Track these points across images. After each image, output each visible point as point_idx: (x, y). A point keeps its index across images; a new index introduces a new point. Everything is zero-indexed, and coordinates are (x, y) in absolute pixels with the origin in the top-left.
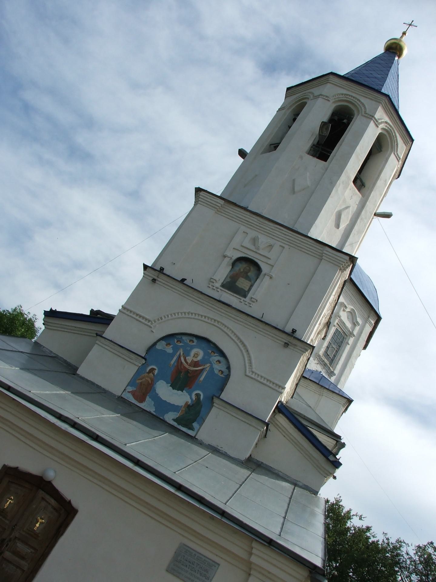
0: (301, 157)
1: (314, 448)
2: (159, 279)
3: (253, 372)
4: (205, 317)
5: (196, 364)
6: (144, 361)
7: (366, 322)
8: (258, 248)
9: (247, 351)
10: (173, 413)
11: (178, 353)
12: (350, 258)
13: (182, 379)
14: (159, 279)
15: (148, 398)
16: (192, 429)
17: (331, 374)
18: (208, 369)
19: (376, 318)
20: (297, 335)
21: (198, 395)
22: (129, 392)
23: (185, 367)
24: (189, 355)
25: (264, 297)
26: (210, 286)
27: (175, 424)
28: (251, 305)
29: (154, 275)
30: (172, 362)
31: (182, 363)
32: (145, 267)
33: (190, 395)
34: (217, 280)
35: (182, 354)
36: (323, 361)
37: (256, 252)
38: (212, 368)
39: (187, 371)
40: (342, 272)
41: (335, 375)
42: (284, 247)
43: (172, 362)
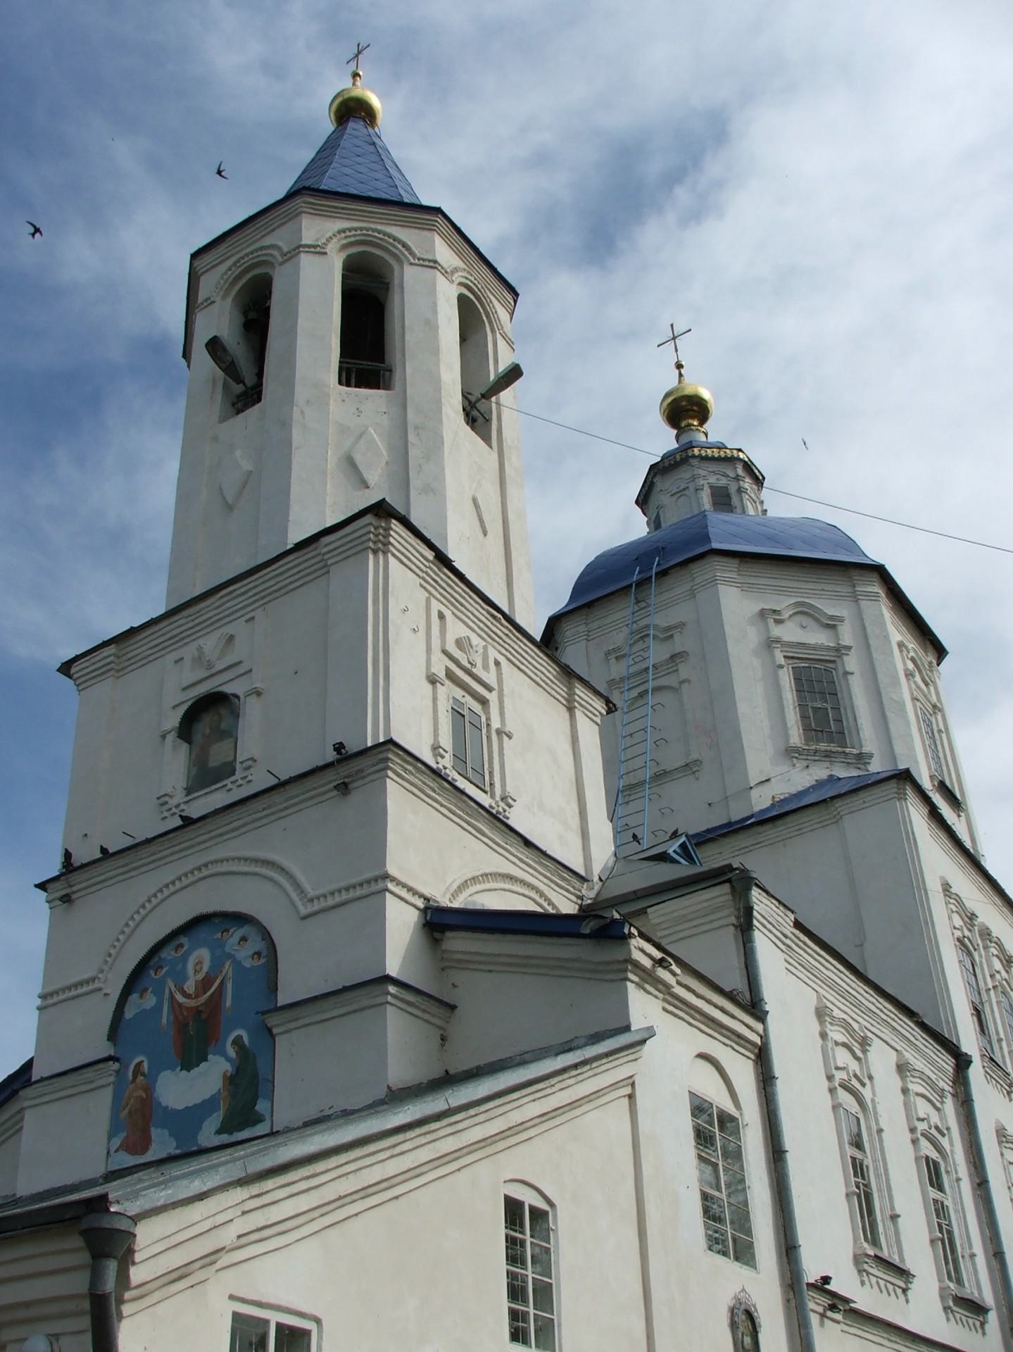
0: (215, 439)
1: (546, 939)
2: (74, 889)
3: (311, 900)
4: (180, 879)
5: (205, 983)
6: (116, 1066)
7: (857, 601)
8: (210, 665)
9: (283, 869)
10: (210, 1119)
11: (167, 991)
12: (377, 515)
13: (194, 1037)
14: (74, 889)
15: (155, 1133)
16: (259, 1119)
17: (862, 759)
18: (230, 974)
19: (875, 577)
20: (352, 747)
21: (238, 1042)
22: (117, 1151)
23: (188, 1009)
24: (186, 978)
25: (269, 742)
26: (166, 814)
27: (225, 1138)
28: (250, 778)
29: (59, 890)
30: (164, 1020)
31: (180, 1005)
32: (42, 886)
33: (224, 1054)
34: (169, 791)
35: (173, 988)
36: (816, 751)
37: (212, 676)
38: (237, 964)
39: (197, 1012)
40: (385, 553)
41: (871, 756)
42: (252, 618)
43: (164, 1020)
